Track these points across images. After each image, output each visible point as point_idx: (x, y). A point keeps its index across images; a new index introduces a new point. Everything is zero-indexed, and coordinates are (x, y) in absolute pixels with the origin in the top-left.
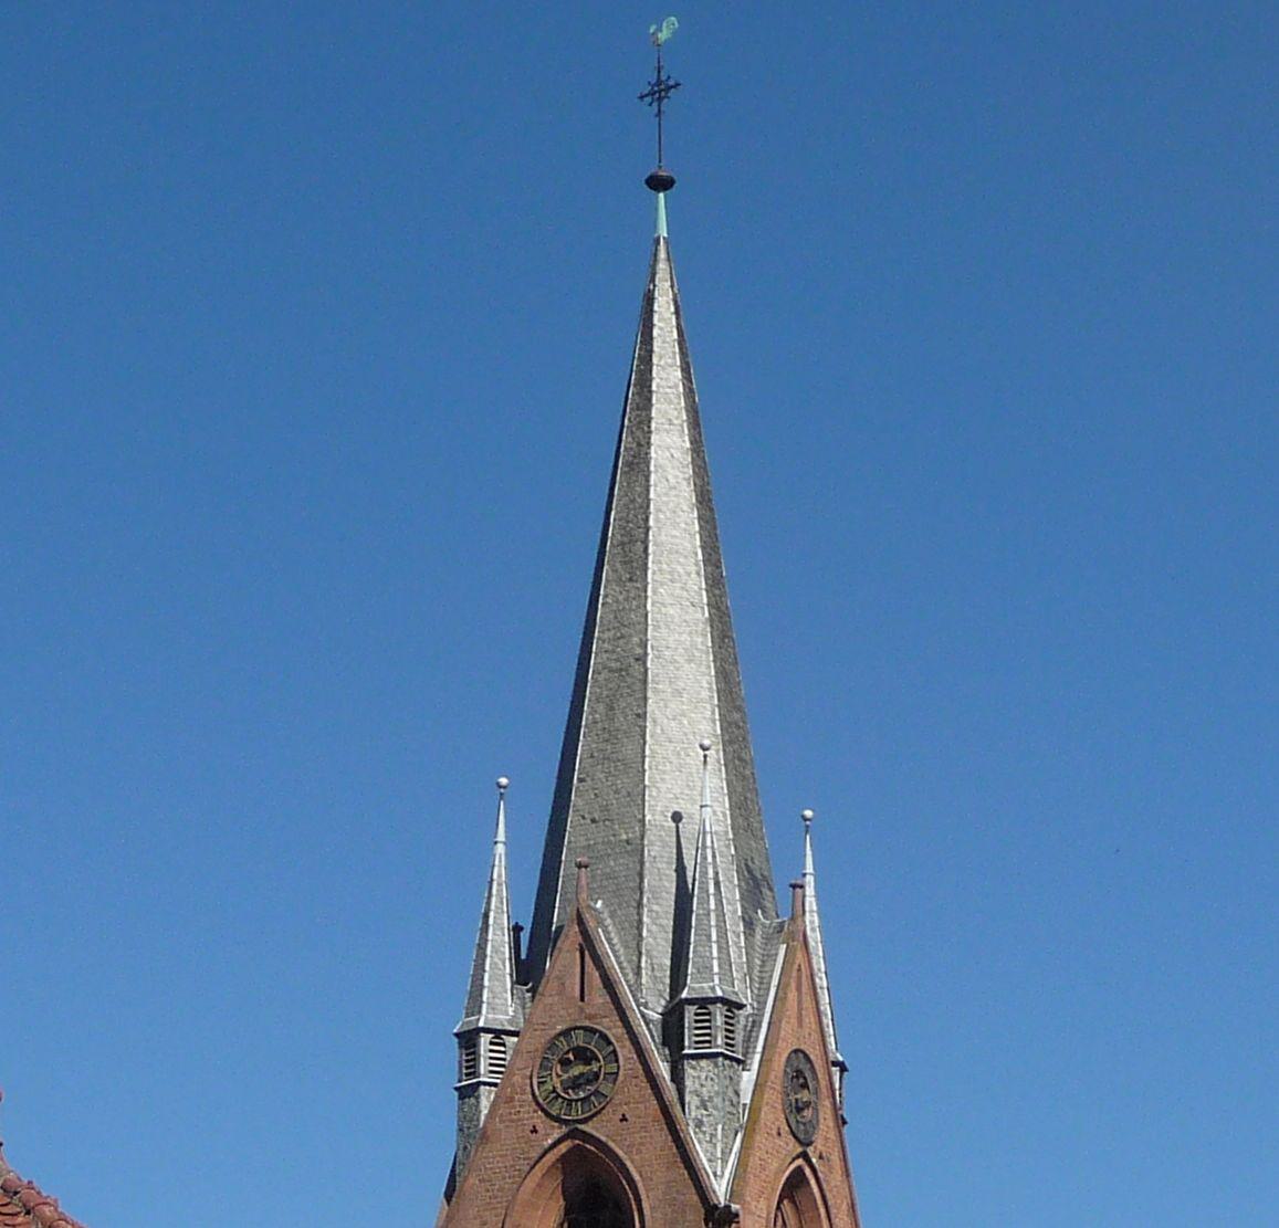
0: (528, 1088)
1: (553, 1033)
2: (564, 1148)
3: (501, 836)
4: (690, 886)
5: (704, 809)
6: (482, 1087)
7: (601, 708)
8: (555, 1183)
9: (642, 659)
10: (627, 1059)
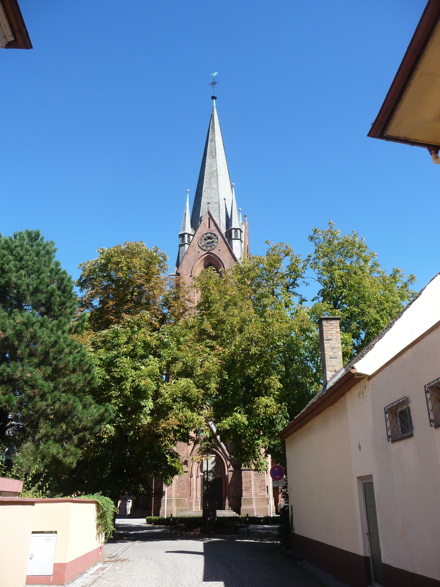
0: (197, 244)
1: (203, 234)
2: (206, 255)
3: (188, 200)
4: (230, 216)
5: (193, 234)
6: (186, 244)
7: (208, 179)
8: (203, 263)
9: (216, 171)
10: (220, 239)
